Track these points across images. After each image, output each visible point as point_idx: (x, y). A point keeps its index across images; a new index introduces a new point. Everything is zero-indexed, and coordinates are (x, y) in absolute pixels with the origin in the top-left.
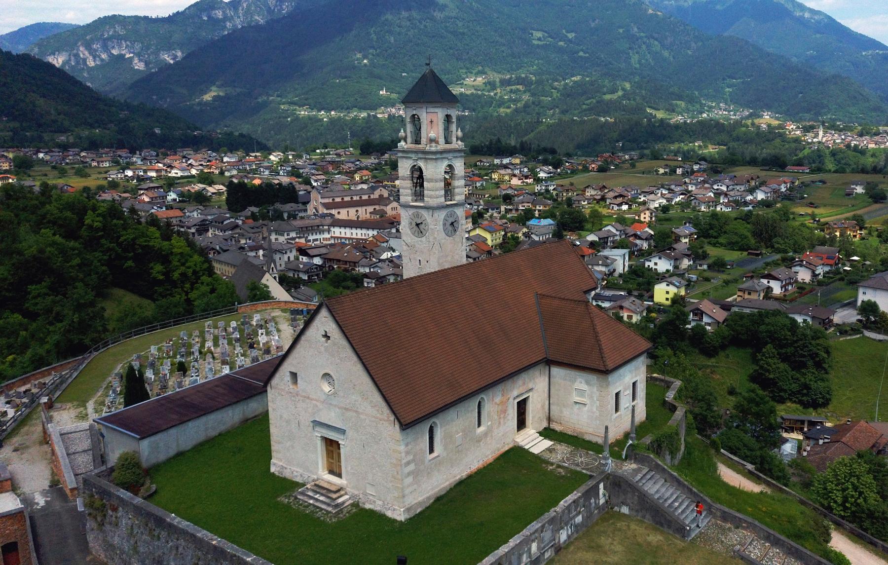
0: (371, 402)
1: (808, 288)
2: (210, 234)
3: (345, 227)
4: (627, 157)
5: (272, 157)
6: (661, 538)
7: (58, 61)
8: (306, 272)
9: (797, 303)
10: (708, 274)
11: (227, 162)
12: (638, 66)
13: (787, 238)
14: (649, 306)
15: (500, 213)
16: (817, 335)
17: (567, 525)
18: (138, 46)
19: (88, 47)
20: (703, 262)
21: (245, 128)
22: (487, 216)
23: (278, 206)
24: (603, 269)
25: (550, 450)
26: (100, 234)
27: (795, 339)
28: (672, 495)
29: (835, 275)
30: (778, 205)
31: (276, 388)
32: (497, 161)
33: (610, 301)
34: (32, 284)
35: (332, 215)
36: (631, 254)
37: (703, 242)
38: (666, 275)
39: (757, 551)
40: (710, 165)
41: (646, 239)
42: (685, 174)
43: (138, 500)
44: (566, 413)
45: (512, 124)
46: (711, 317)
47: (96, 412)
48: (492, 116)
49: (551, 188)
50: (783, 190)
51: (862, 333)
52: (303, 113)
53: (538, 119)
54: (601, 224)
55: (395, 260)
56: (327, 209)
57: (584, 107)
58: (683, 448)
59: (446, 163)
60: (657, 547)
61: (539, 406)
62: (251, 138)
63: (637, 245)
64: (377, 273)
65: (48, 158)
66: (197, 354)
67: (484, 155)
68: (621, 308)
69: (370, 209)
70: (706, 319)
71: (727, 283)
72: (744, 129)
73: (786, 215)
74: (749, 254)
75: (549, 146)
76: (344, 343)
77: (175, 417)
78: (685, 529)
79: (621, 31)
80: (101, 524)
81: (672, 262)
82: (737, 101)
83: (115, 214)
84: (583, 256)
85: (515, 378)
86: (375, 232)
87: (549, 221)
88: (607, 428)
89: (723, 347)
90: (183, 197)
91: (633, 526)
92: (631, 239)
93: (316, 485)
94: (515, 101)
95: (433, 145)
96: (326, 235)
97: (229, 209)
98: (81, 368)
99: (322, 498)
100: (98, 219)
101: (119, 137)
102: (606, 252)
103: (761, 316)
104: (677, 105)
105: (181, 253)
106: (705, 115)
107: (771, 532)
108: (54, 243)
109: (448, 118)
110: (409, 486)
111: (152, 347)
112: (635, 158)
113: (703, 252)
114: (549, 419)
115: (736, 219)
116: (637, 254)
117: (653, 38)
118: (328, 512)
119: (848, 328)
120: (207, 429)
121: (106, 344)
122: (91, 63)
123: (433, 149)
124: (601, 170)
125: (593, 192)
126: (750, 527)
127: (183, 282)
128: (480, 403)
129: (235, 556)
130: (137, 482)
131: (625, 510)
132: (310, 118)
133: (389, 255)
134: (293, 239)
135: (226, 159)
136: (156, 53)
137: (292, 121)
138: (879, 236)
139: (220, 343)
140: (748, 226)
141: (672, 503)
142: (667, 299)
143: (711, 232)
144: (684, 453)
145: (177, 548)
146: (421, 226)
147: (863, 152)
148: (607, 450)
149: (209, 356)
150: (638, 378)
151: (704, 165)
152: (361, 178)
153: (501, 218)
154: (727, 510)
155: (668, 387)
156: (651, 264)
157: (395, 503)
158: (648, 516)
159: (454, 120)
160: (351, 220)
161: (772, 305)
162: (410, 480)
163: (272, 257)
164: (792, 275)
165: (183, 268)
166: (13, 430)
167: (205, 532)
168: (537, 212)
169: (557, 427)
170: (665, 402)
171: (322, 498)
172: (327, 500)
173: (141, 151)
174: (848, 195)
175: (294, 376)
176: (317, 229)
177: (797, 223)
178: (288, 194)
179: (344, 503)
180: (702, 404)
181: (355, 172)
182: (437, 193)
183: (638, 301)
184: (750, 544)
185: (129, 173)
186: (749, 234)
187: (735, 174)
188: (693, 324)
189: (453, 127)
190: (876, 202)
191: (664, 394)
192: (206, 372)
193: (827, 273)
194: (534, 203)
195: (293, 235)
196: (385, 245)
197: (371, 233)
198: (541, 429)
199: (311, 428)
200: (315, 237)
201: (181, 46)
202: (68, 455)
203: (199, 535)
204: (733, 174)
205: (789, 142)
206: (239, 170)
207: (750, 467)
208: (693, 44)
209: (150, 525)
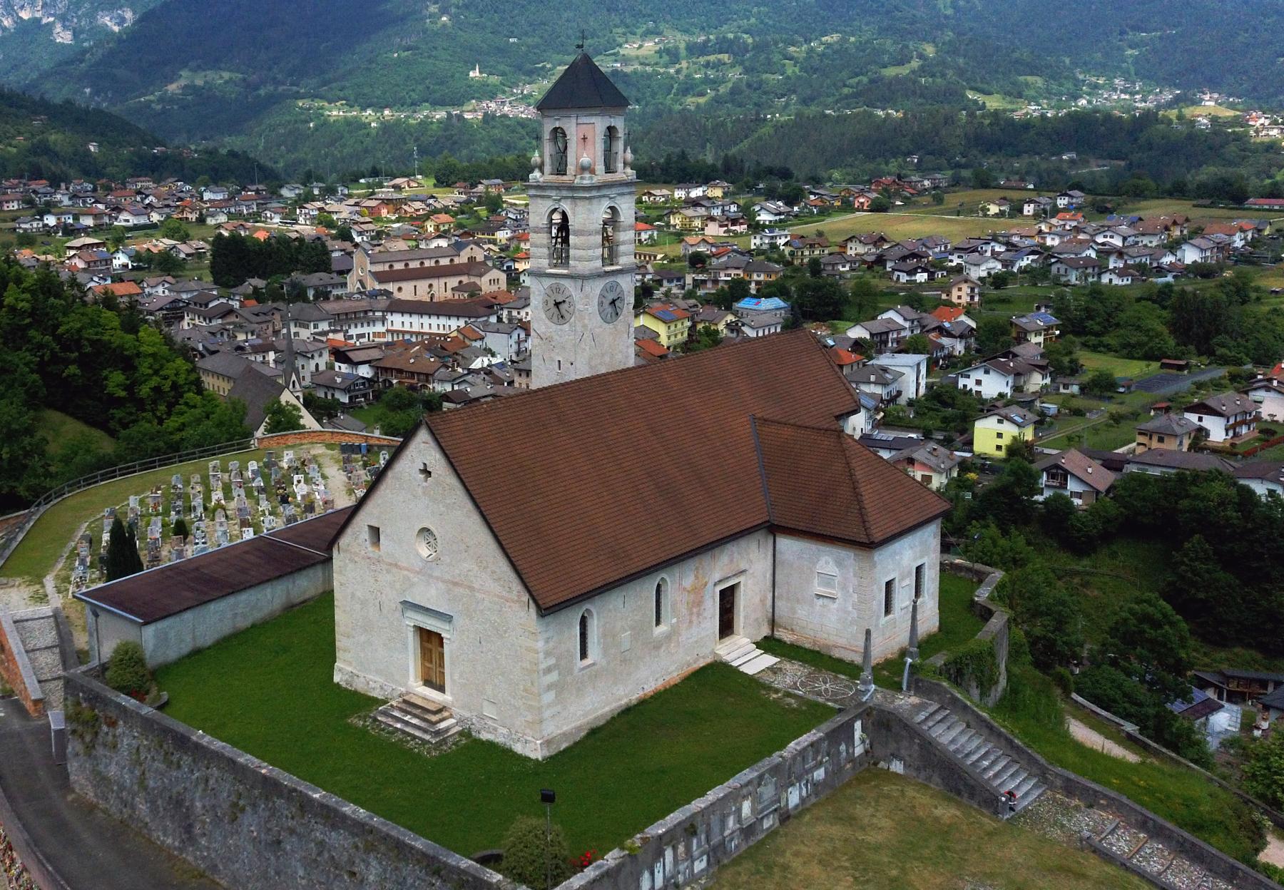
0: (494, 572)
2: (185, 324)
3: (411, 314)
4: (926, 183)
6: (958, 813)
8: (346, 390)
9: (1256, 460)
10: (1080, 403)
11: (210, 201)
12: (950, 12)
13: (1243, 336)
15: (683, 287)
17: (800, 781)
20: (1071, 379)
21: (231, 142)
22: (658, 294)
24: (878, 390)
26: (27, 321)
27: (1250, 526)
28: (978, 748)
30: (1227, 274)
31: (346, 551)
32: (679, 194)
33: (890, 449)
35: (388, 294)
36: (932, 364)
38: (999, 404)
39: (1122, 843)
40: (1090, 198)
41: (961, 337)
42: (1041, 215)
43: (147, 710)
44: (802, 612)
45: (709, 124)
46: (1083, 483)
47: (59, 592)
48: (670, 110)
50: (1238, 243)
52: (336, 113)
53: (758, 114)
54: (875, 309)
55: (495, 370)
56: (380, 282)
57: (846, 90)
58: (1003, 682)
59: (606, 203)
60: (949, 826)
62: (248, 159)
63: (942, 347)
64: (466, 393)
66: (200, 510)
67: (655, 182)
68: (911, 461)
69: (453, 282)
70: (1072, 486)
71: (1117, 419)
72: (1161, 127)
73: (1241, 292)
75: (778, 163)
76: (452, 481)
77: (188, 594)
78: (998, 800)
80: (90, 748)
81: (1011, 380)
82: (1149, 73)
83: (49, 290)
84: (841, 367)
85: (717, 551)
86: (462, 323)
87: (775, 302)
88: (868, 632)
89: (1106, 538)
90: (139, 261)
91: (910, 792)
92: (932, 336)
93: (405, 701)
94: (714, 83)
95: (587, 175)
96: (379, 328)
97: (216, 282)
98: (28, 526)
99: (415, 721)
100: (24, 296)
102: (884, 360)
103: (1183, 482)
104: (1027, 85)
105: (154, 355)
106: (1082, 102)
107: (1151, 815)
110: (549, 706)
111: (132, 498)
112: (944, 184)
113: (1071, 361)
114: (773, 623)
115: (1139, 300)
116: (941, 364)
118: (424, 742)
123: (586, 182)
125: (861, 249)
126: (1113, 805)
127: (154, 402)
128: (659, 586)
129: (295, 790)
130: (140, 687)
131: (897, 767)
132: (348, 122)
133: (486, 363)
134: (325, 333)
135: (207, 196)
136: (91, 15)
137: (316, 128)
139: (235, 494)
140: (1165, 313)
141: (978, 761)
142: (999, 448)
143: (1089, 323)
144: (1005, 690)
145: (207, 781)
146: (563, 307)
148: (867, 674)
149: (220, 513)
150: (925, 560)
151: (1079, 197)
152: (437, 228)
153: (685, 297)
154: (1072, 776)
155: (980, 581)
156: (970, 383)
157: (528, 731)
158: (936, 778)
160: (420, 302)
161: (1206, 462)
162: (550, 697)
163: (293, 364)
164: (1249, 407)
167: (249, 756)
168: (753, 285)
170: (973, 604)
171: (415, 721)
172: (423, 724)
175: (375, 532)
176: (363, 316)
177: (1266, 309)
178: (312, 256)
179: (448, 729)
180: (1046, 620)
181: (427, 217)
182: (590, 252)
184: (1112, 832)
185: (51, 220)
186: (1164, 330)
187: (1141, 214)
188: (1048, 493)
189: (619, 145)
191: (973, 591)
192: (215, 536)
194: (748, 269)
195: (324, 326)
196: (478, 344)
198: (759, 639)
199: (398, 614)
200: (360, 330)
202: (27, 652)
203: (241, 760)
204: (1136, 214)
205: (1255, 151)
206: (231, 216)
207: (1130, 728)
209: (165, 746)
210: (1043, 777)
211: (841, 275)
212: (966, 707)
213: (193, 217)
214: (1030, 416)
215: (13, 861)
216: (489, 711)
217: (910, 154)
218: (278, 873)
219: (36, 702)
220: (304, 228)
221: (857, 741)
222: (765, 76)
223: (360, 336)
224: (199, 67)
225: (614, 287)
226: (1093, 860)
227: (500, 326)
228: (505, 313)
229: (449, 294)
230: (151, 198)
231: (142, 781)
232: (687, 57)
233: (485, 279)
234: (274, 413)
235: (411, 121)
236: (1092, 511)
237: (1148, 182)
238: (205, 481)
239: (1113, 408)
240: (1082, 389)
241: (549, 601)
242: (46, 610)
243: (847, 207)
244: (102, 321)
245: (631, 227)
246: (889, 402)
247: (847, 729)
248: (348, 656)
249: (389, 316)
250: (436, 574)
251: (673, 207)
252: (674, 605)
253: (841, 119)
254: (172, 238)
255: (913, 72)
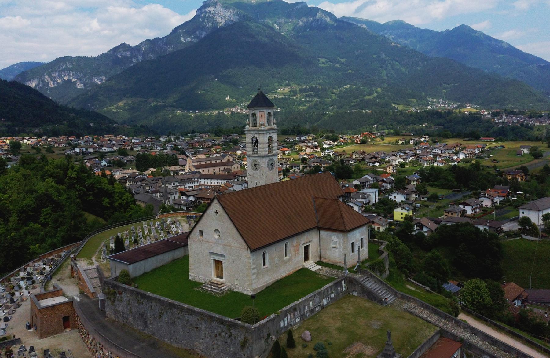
1: (489, 211)
3: (207, 179)
5: (161, 139)
7: (33, 84)
8: (185, 205)
10: (428, 203)
12: (385, 78)
14: (390, 222)
16: (493, 237)
18: (79, 74)
19: (50, 76)
20: (425, 196)
23: (167, 167)
24: (362, 200)
25: (320, 270)
29: (507, 203)
32: (298, 138)
34: (43, 208)
35: (199, 172)
36: (380, 192)
37: (425, 184)
41: (390, 183)
43: (132, 288)
46: (428, 228)
49: (331, 154)
51: (521, 236)
57: (352, 104)
61: (315, 250)
63: (383, 187)
65: (29, 142)
66: (141, 237)
69: (222, 168)
70: (424, 229)
71: (439, 208)
74: (453, 191)
79: (375, 56)
80: (113, 302)
82: (450, 98)
85: (303, 234)
86: (225, 182)
88: (345, 255)
91: (358, 300)
92: (380, 183)
93: (211, 282)
96: (196, 184)
101: (70, 129)
102: (364, 191)
103: (458, 226)
104: (411, 101)
105: (119, 192)
108: (52, 187)
109: (269, 114)
113: (425, 190)
114: (320, 257)
117: (395, 60)
118: (217, 293)
119: (512, 233)
120: (157, 262)
121: (94, 233)
122: (52, 85)
123: (262, 129)
124: (363, 142)
125: (357, 156)
131: (355, 294)
132: (183, 115)
134: (177, 186)
135: (133, 141)
137: (172, 117)
138: (537, 179)
142: (402, 218)
143: (431, 178)
145: (152, 307)
146: (257, 166)
147: (532, 128)
152: (216, 150)
156: (393, 198)
159: (272, 115)
161: (464, 220)
162: (254, 277)
165: (120, 201)
166: (55, 272)
168: (322, 168)
169: (324, 261)
173: (83, 137)
174: (519, 154)
175: (201, 232)
176: (191, 180)
177: (485, 172)
179: (224, 289)
181: (212, 147)
183: (383, 219)
185: (77, 150)
186: (453, 179)
187: (447, 143)
188: (417, 232)
189: (272, 118)
190: (536, 158)
193: (502, 201)
195: (177, 184)
197: (223, 182)
199: (208, 256)
200: (190, 185)
201: (105, 74)
203: (162, 299)
207: (427, 288)
208: (420, 63)
210: (396, 295)
211: (351, 164)
212: (374, 277)
213: (129, 148)
214: (411, 207)
215: (89, 338)
216: (236, 283)
217: (374, 125)
218: (174, 332)
219: (93, 293)
220: (169, 150)
221: (343, 287)
222: (325, 99)
223: (190, 187)
224: (130, 96)
225: (272, 160)
226: (407, 314)
227: (239, 182)
228: (240, 178)
229: (221, 172)
230: (113, 142)
231: (130, 311)
232: (300, 93)
233: (233, 167)
234: (163, 209)
235: (206, 115)
236: (431, 237)
237: (449, 133)
238: (142, 228)
239: (438, 204)
240: (428, 199)
241: (254, 248)
242: (93, 267)
243: (353, 142)
244: (102, 181)
245: (276, 142)
246: (366, 204)
247: (340, 283)
248: (193, 269)
249: (200, 180)
250: (220, 243)
251: (296, 143)
252: (290, 250)
253: (351, 113)
254: (121, 155)
255: (374, 97)
